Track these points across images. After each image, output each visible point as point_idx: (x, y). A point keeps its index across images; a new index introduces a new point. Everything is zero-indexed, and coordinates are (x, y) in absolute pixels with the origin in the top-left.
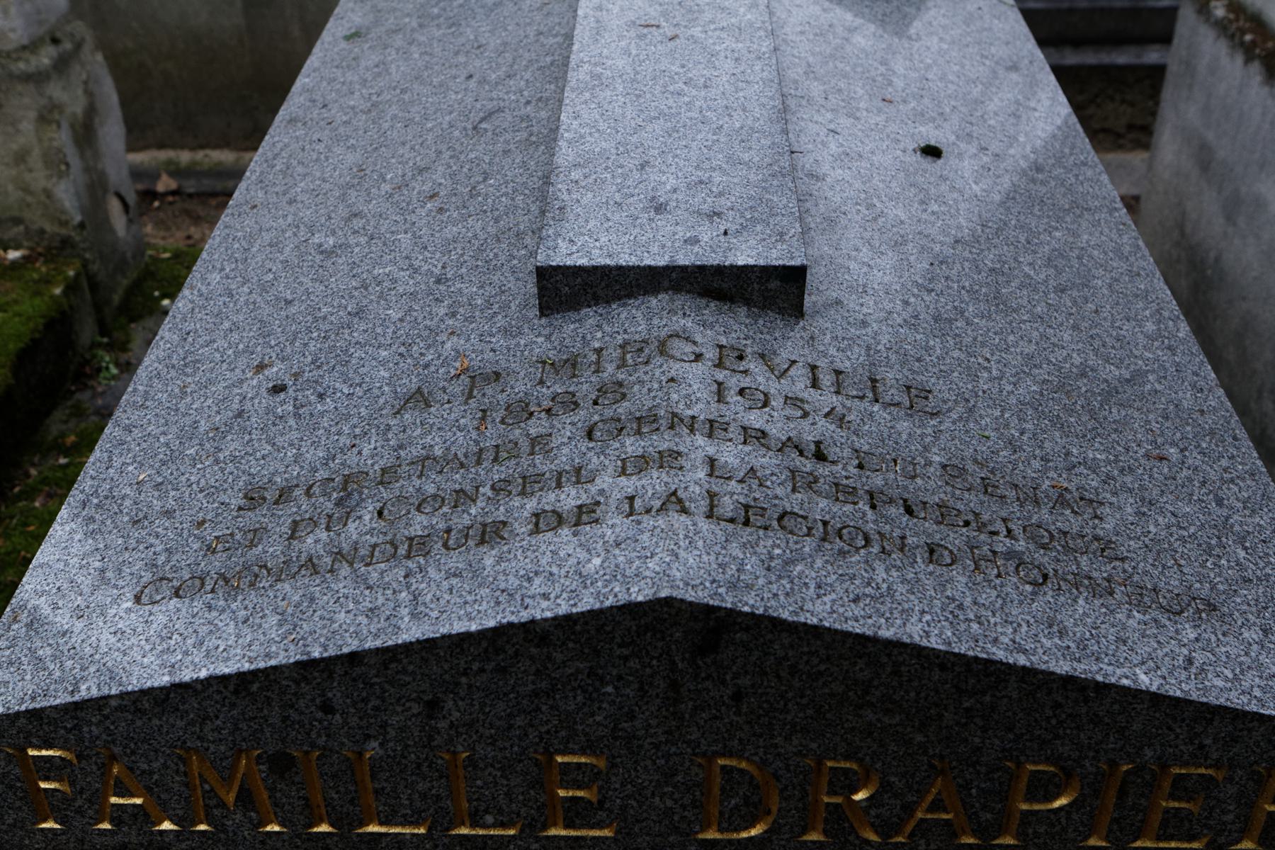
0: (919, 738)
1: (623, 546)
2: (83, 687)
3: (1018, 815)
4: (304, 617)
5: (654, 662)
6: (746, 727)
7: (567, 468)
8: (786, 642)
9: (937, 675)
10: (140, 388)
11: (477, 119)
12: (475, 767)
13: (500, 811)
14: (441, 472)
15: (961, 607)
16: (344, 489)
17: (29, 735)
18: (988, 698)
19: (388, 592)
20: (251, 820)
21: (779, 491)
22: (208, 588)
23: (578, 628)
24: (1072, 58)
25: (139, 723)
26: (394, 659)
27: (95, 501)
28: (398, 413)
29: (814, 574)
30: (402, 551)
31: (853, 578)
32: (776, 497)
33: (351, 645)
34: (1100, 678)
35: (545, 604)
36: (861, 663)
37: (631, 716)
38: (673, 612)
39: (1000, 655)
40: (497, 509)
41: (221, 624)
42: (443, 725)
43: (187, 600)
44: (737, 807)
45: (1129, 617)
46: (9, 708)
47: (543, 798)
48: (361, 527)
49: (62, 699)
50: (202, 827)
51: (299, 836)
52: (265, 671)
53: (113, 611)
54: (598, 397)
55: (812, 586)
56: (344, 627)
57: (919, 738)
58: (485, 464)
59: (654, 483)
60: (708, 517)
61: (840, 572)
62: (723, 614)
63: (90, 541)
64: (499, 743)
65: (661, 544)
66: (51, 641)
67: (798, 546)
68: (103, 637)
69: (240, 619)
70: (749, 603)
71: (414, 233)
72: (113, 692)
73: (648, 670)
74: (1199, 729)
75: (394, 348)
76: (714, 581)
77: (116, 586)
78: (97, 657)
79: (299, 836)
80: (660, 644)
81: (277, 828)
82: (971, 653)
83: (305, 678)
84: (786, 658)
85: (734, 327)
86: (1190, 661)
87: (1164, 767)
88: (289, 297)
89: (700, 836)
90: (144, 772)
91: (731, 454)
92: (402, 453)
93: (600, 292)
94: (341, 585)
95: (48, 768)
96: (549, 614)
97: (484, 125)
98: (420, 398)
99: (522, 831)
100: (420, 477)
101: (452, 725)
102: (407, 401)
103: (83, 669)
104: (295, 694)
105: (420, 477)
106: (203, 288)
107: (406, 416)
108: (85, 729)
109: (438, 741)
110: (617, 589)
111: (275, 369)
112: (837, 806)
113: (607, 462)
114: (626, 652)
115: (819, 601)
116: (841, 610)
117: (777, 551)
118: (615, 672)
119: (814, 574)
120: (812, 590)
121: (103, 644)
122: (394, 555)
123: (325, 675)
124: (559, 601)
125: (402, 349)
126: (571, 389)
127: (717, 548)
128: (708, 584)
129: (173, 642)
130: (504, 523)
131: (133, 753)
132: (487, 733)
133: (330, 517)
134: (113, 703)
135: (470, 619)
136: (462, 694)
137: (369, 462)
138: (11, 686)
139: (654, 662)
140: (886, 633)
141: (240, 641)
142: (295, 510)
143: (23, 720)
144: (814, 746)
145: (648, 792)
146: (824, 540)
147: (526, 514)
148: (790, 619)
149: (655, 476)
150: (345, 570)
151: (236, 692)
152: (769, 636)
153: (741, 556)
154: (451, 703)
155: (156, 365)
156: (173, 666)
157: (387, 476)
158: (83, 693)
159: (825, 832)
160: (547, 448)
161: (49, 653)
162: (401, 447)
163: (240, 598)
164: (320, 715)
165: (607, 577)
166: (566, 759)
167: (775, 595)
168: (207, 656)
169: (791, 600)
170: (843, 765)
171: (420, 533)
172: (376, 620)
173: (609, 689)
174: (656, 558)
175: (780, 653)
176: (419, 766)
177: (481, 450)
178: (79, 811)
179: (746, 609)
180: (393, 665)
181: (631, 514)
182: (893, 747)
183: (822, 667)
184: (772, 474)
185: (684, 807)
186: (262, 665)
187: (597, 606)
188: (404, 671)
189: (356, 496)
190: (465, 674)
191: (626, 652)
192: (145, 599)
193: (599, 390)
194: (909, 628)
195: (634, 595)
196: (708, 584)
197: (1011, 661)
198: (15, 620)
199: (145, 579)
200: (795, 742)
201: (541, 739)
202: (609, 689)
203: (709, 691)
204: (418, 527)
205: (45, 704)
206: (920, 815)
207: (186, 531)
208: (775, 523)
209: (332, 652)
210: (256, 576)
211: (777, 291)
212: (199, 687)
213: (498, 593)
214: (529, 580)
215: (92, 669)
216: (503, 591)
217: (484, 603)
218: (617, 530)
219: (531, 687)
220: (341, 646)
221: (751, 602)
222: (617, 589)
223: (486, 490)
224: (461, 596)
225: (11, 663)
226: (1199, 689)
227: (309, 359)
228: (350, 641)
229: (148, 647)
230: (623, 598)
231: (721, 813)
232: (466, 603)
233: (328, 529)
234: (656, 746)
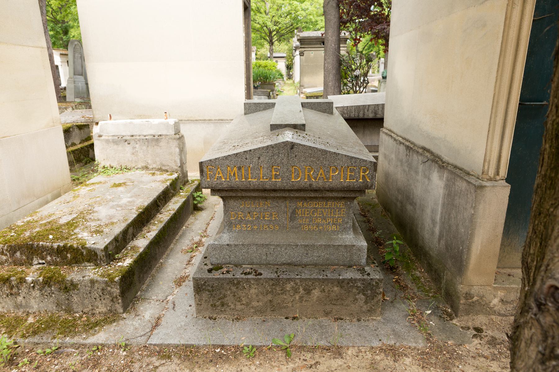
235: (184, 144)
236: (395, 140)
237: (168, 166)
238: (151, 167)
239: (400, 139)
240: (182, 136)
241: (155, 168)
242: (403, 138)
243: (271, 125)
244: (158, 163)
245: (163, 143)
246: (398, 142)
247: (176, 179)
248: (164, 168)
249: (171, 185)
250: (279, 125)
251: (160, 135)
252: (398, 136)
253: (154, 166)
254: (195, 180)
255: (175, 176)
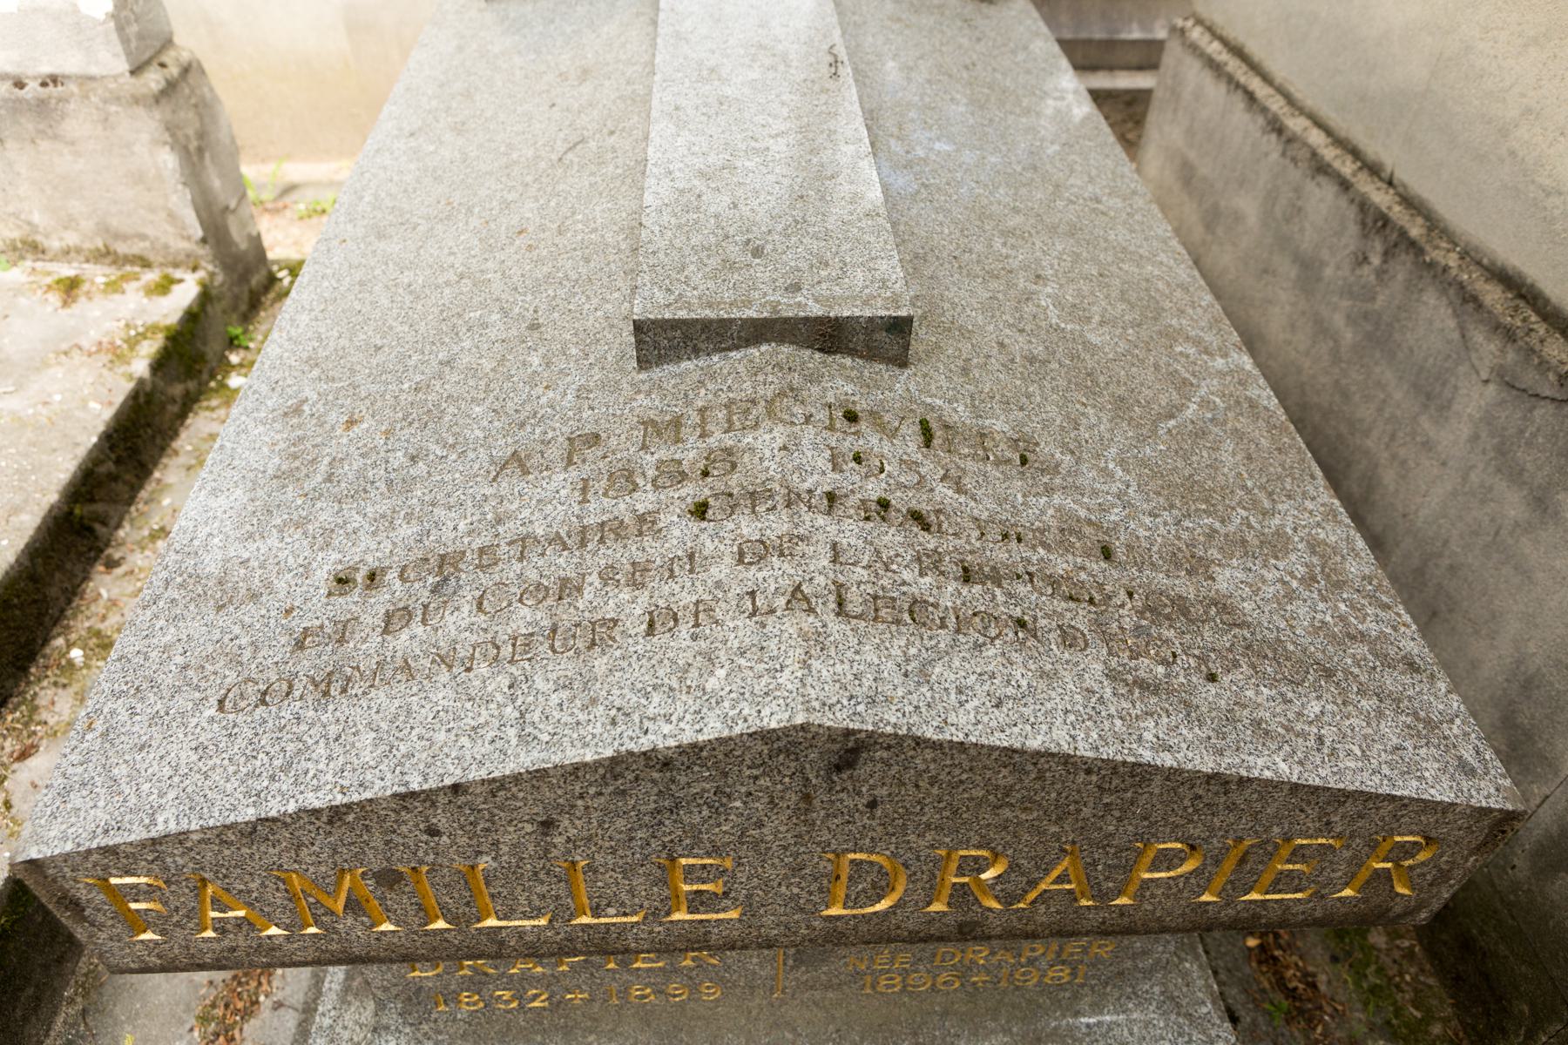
0: (1054, 829)
1: (748, 655)
2: (160, 819)
3: (1138, 882)
4: (400, 735)
5: (787, 780)
6: (879, 829)
7: (680, 553)
8: (929, 757)
9: (1081, 777)
10: (228, 445)
11: (562, 150)
12: (596, 872)
13: (623, 904)
14: (543, 554)
15: (1101, 700)
16: (440, 573)
17: (106, 868)
18: (1129, 795)
19: (492, 706)
20: (363, 923)
21: (907, 575)
22: (297, 694)
23: (704, 754)
24: (1103, 81)
25: (227, 852)
26: (502, 787)
27: (179, 580)
28: (494, 480)
29: (953, 677)
30: (507, 651)
31: (993, 676)
32: (904, 583)
33: (454, 775)
34: (1244, 773)
35: (666, 729)
36: (1005, 772)
37: (760, 825)
38: (809, 736)
39: (1147, 756)
40: (606, 603)
41: (310, 742)
42: (558, 840)
43: (274, 709)
44: (864, 890)
45: (1257, 693)
46: (79, 845)
47: (666, 893)
48: (458, 621)
49: (138, 834)
50: (313, 930)
51: (416, 933)
52: (361, 805)
53: (194, 721)
54: (706, 466)
55: (953, 692)
56: (446, 750)
57: (1054, 829)
58: (590, 546)
59: (776, 575)
60: (838, 615)
61: (979, 670)
62: (863, 735)
63: (172, 630)
64: (620, 852)
65: (791, 653)
66: (127, 757)
67: (933, 643)
68: (183, 755)
69: (332, 736)
70: (891, 720)
71: (503, 274)
72: (193, 827)
73: (779, 787)
74: (1330, 809)
75: (487, 402)
76: (851, 697)
77: (197, 688)
78: (176, 779)
79: (416, 933)
80: (793, 764)
81: (392, 928)
82: (1119, 758)
83: (405, 808)
84: (927, 770)
85: (842, 380)
86: (1320, 739)
87: (1288, 840)
88: (379, 343)
89: (825, 913)
90: (241, 891)
91: (850, 532)
92: (501, 529)
93: (702, 346)
94: (440, 696)
95: (136, 893)
96: (672, 743)
97: (570, 156)
98: (518, 462)
99: (645, 918)
100: (521, 559)
101: (569, 840)
102: (503, 467)
103: (161, 795)
104: (396, 821)
105: (521, 559)
106: (293, 333)
107: (504, 484)
108: (169, 860)
109: (555, 853)
110: (746, 712)
111: (365, 425)
112: (963, 885)
113: (722, 547)
114: (755, 772)
115: (961, 710)
116: (986, 719)
117: (913, 651)
118: (743, 790)
119: (953, 677)
120: (953, 696)
121: (183, 762)
122: (496, 659)
123: (428, 804)
124: (682, 725)
125: (497, 405)
126: (677, 457)
127: (849, 654)
128: (845, 702)
129: (258, 763)
130: (615, 622)
131: (225, 876)
132: (607, 844)
133: (426, 607)
134: (195, 837)
135: (586, 745)
136: (578, 814)
137: (466, 540)
138: (82, 814)
139: (787, 780)
140: (1034, 744)
141: (332, 765)
142: (387, 597)
143: (95, 857)
144: (947, 840)
145: (775, 884)
146: (958, 631)
147: (639, 611)
148: (935, 737)
149: (776, 566)
150: (444, 677)
151: (330, 822)
152: (912, 753)
153: (876, 661)
154: (567, 822)
155: (243, 418)
156: (258, 795)
157: (487, 557)
158: (161, 827)
159: (949, 904)
160: (656, 528)
161: (125, 772)
162: (499, 521)
163: (331, 707)
164: (425, 837)
165: (733, 695)
166: (691, 861)
167: (917, 707)
168: (295, 783)
169: (934, 713)
170: (973, 853)
171: (524, 631)
172: (480, 742)
173: (738, 804)
174: (787, 671)
175: (922, 767)
176: (536, 874)
177: (584, 527)
178: (178, 925)
179: (889, 729)
180: (502, 793)
181: (753, 614)
182: (1026, 837)
183: (964, 776)
184: (897, 555)
185: (810, 893)
186: (356, 798)
187: (726, 733)
188: (514, 797)
189: (453, 581)
190: (581, 797)
191: (755, 772)
192: (228, 705)
193: (707, 459)
194: (1055, 734)
195: (766, 720)
196: (845, 702)
197: (1159, 763)
198: (90, 728)
199: (228, 680)
200: (928, 837)
201: (665, 847)
202: (738, 804)
203: (842, 801)
204: (520, 623)
205: (118, 840)
206: (1043, 886)
207: (272, 621)
208: (906, 617)
209: (432, 783)
210: (349, 679)
211: (887, 340)
212: (289, 820)
213: (614, 712)
214: (647, 696)
215: (171, 795)
216: (619, 709)
217: (599, 724)
218: (740, 634)
219: (653, 806)
220: (442, 776)
221: (893, 720)
222: (746, 712)
223: (594, 578)
224: (572, 714)
225: (84, 784)
226: (1335, 774)
227: (400, 415)
228: (452, 768)
229: (231, 769)
230: (755, 725)
231: (847, 896)
232: (578, 723)
233: (424, 622)
234: (785, 848)
235: (205, 108)
236: (1276, 127)
237: (143, 237)
238: (55, 244)
239: (1316, 138)
240: (186, 70)
241: (78, 251)
242: (1339, 142)
243: (639, 327)
244: (88, 225)
245: (79, 123)
246: (1304, 154)
247: (193, 317)
248: (122, 248)
249: (158, 366)
250: (706, 325)
251: (54, 80)
252: (1290, 100)
253: (72, 239)
254: (292, 283)
255: (186, 293)
